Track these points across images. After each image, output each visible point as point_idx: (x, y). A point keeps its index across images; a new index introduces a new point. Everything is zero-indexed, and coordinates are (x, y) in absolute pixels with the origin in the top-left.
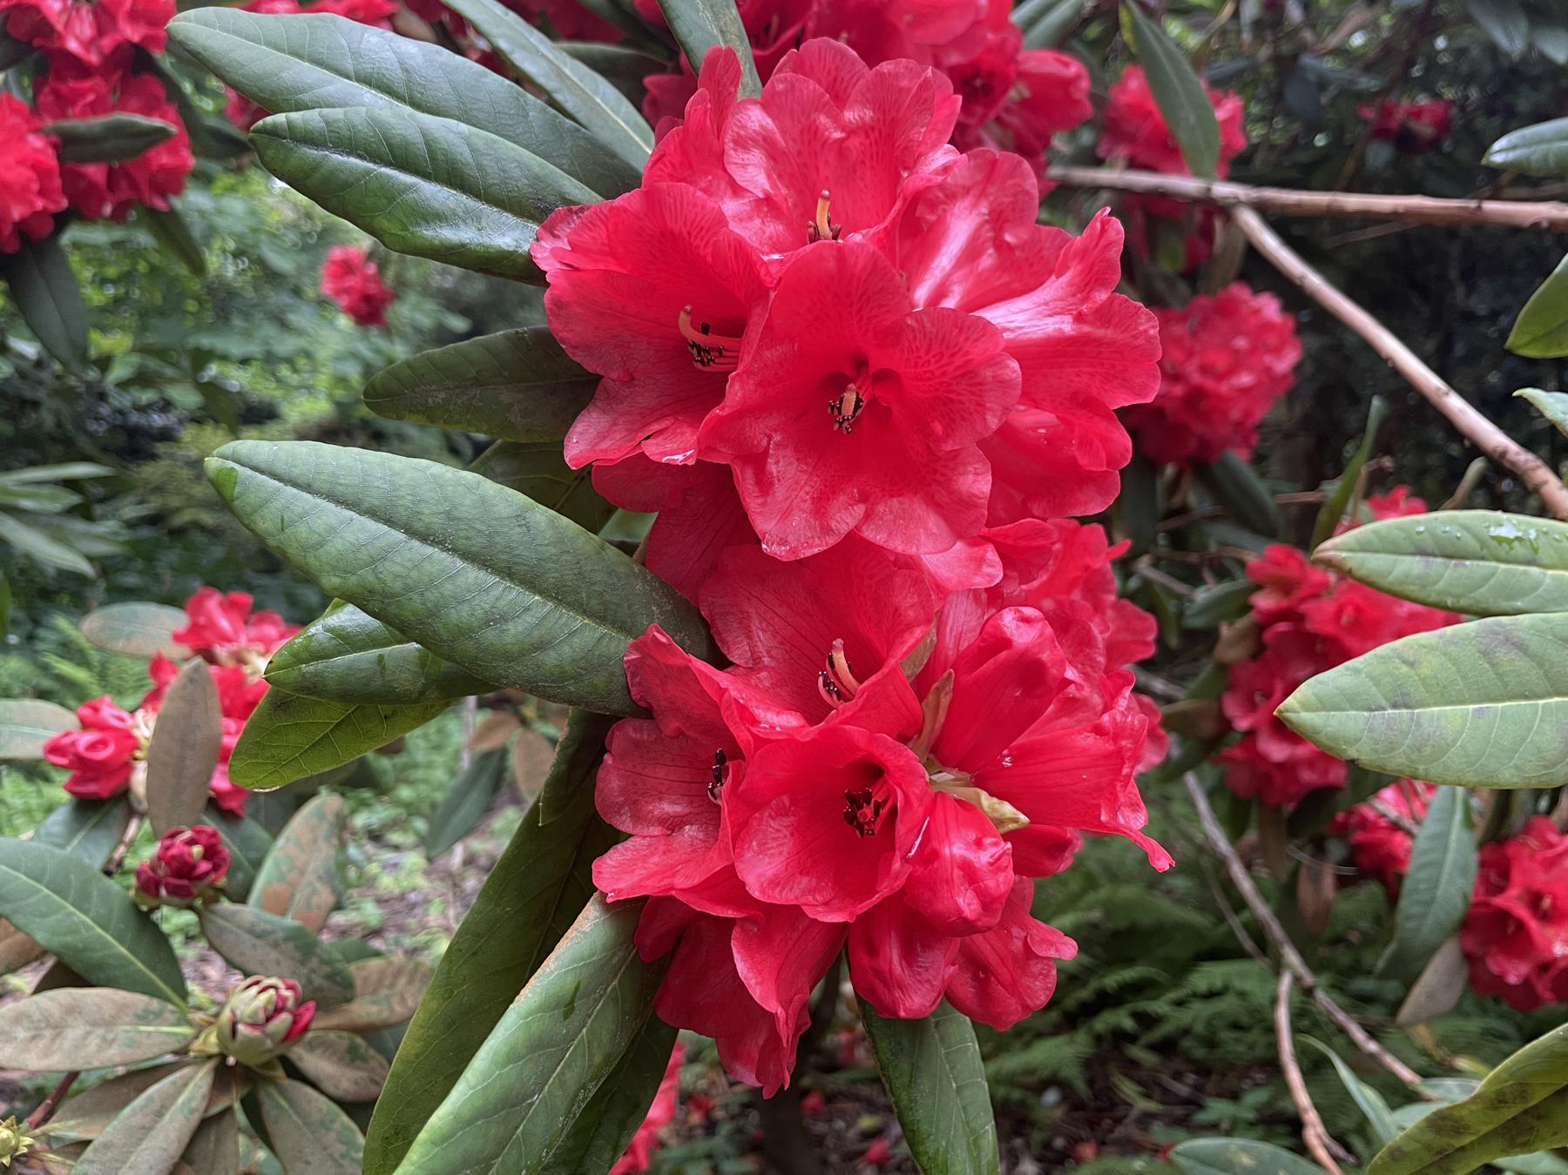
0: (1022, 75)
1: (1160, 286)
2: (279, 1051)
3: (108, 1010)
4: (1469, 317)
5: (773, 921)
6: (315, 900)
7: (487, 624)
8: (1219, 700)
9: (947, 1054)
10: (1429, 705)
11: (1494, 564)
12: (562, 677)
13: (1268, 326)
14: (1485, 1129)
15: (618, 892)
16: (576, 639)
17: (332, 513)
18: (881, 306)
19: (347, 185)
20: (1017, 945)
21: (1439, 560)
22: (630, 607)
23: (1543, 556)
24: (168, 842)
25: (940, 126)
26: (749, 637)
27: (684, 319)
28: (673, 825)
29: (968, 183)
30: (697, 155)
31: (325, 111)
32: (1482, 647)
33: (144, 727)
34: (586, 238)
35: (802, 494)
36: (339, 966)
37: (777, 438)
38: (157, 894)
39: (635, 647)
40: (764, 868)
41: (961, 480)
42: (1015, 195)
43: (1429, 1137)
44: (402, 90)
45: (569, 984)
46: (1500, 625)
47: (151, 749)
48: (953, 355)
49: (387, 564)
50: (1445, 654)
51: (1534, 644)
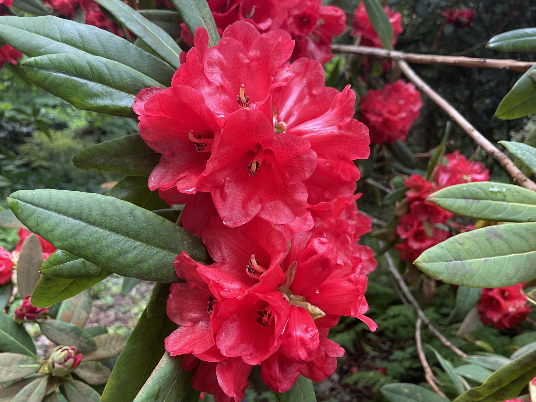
0: (321, 16)
1: (373, 82)
2: (71, 371)
3: (8, 360)
4: (480, 83)
5: (231, 363)
6: (81, 316)
7: (120, 255)
8: (395, 228)
9: (300, 386)
10: (468, 259)
11: (490, 201)
12: (150, 272)
13: (411, 95)
14: (487, 395)
15: (174, 351)
16: (156, 256)
17: (57, 217)
18: (264, 133)
19: (59, 85)
20: (323, 353)
21: (471, 200)
22: (175, 243)
23: (507, 198)
24: (25, 301)
25: (287, 51)
26: (221, 251)
27: (191, 136)
28: (195, 322)
29: (299, 71)
30: (194, 71)
31: (50, 55)
32: (487, 238)
33: (15, 257)
34: (151, 106)
35: (238, 200)
36: (90, 339)
37: (228, 179)
38: (23, 319)
39: (178, 258)
40: (227, 343)
41: (297, 195)
42: (316, 76)
43: (468, 398)
44: (79, 44)
45: (157, 388)
46: (493, 229)
47: (18, 267)
48: (292, 150)
49: (80, 236)
50: (473, 240)
51: (505, 235)
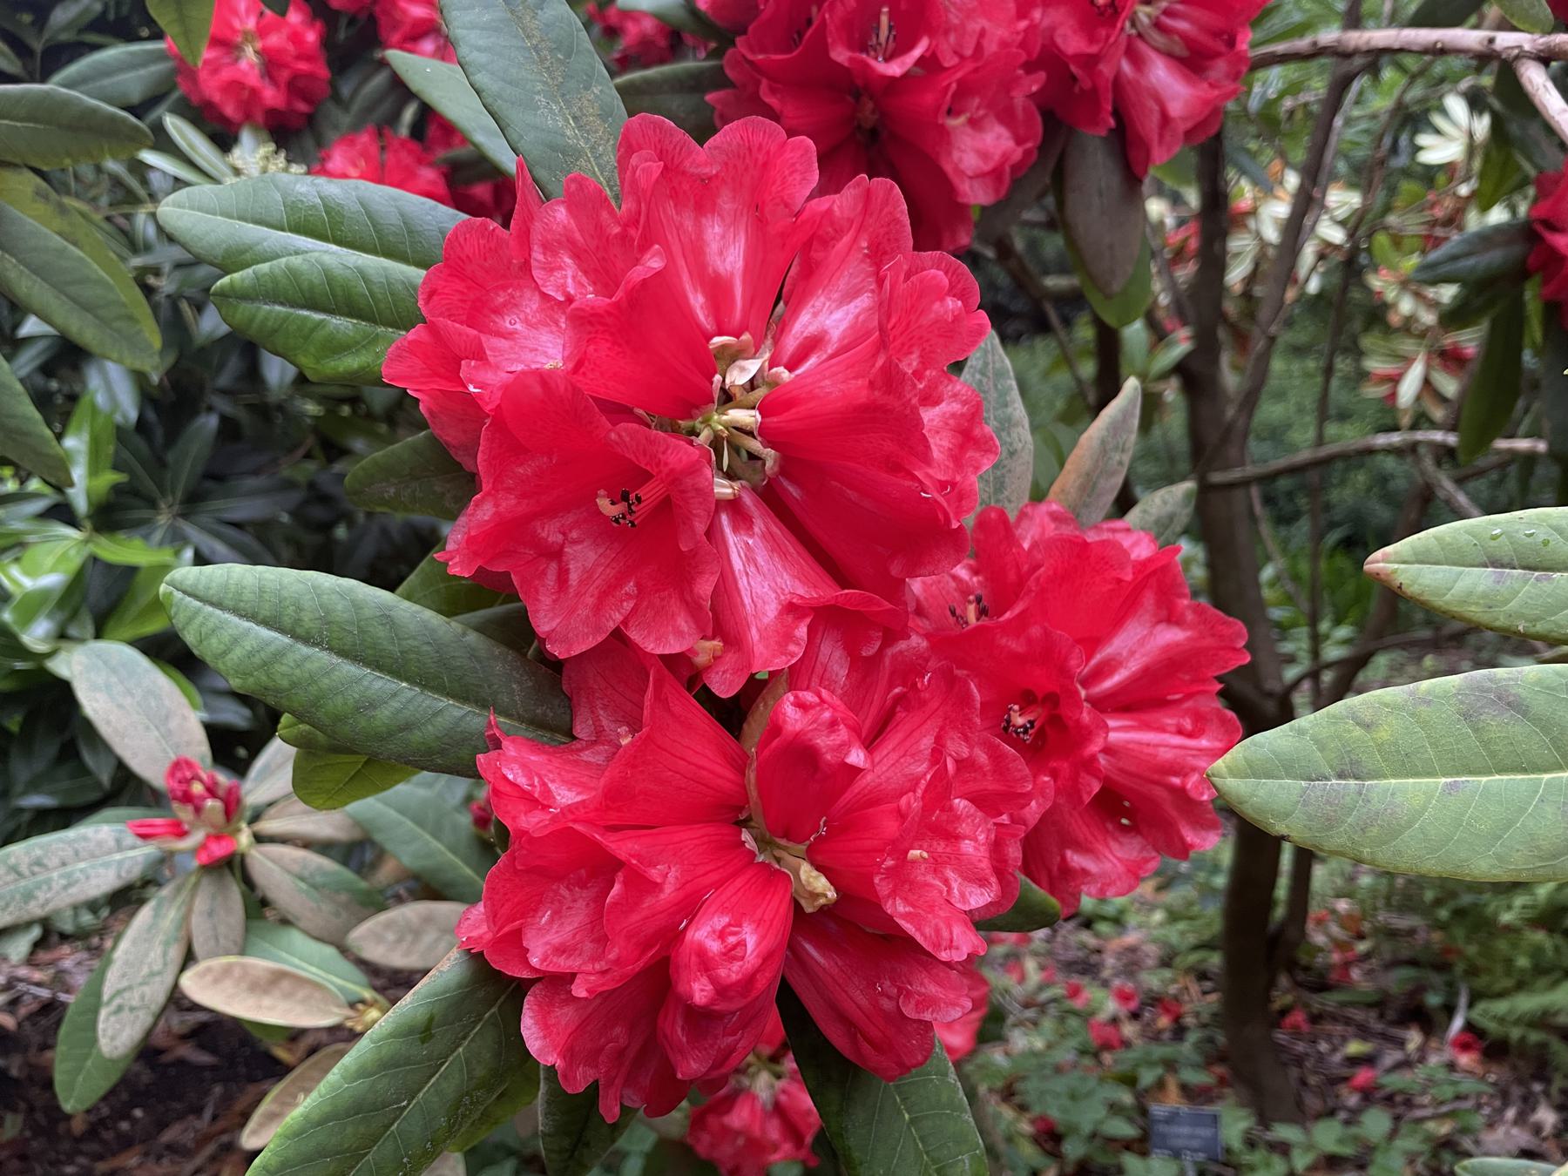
10: (1385, 777)
49: (277, 666)
50: (1412, 715)
51: (1539, 705)
